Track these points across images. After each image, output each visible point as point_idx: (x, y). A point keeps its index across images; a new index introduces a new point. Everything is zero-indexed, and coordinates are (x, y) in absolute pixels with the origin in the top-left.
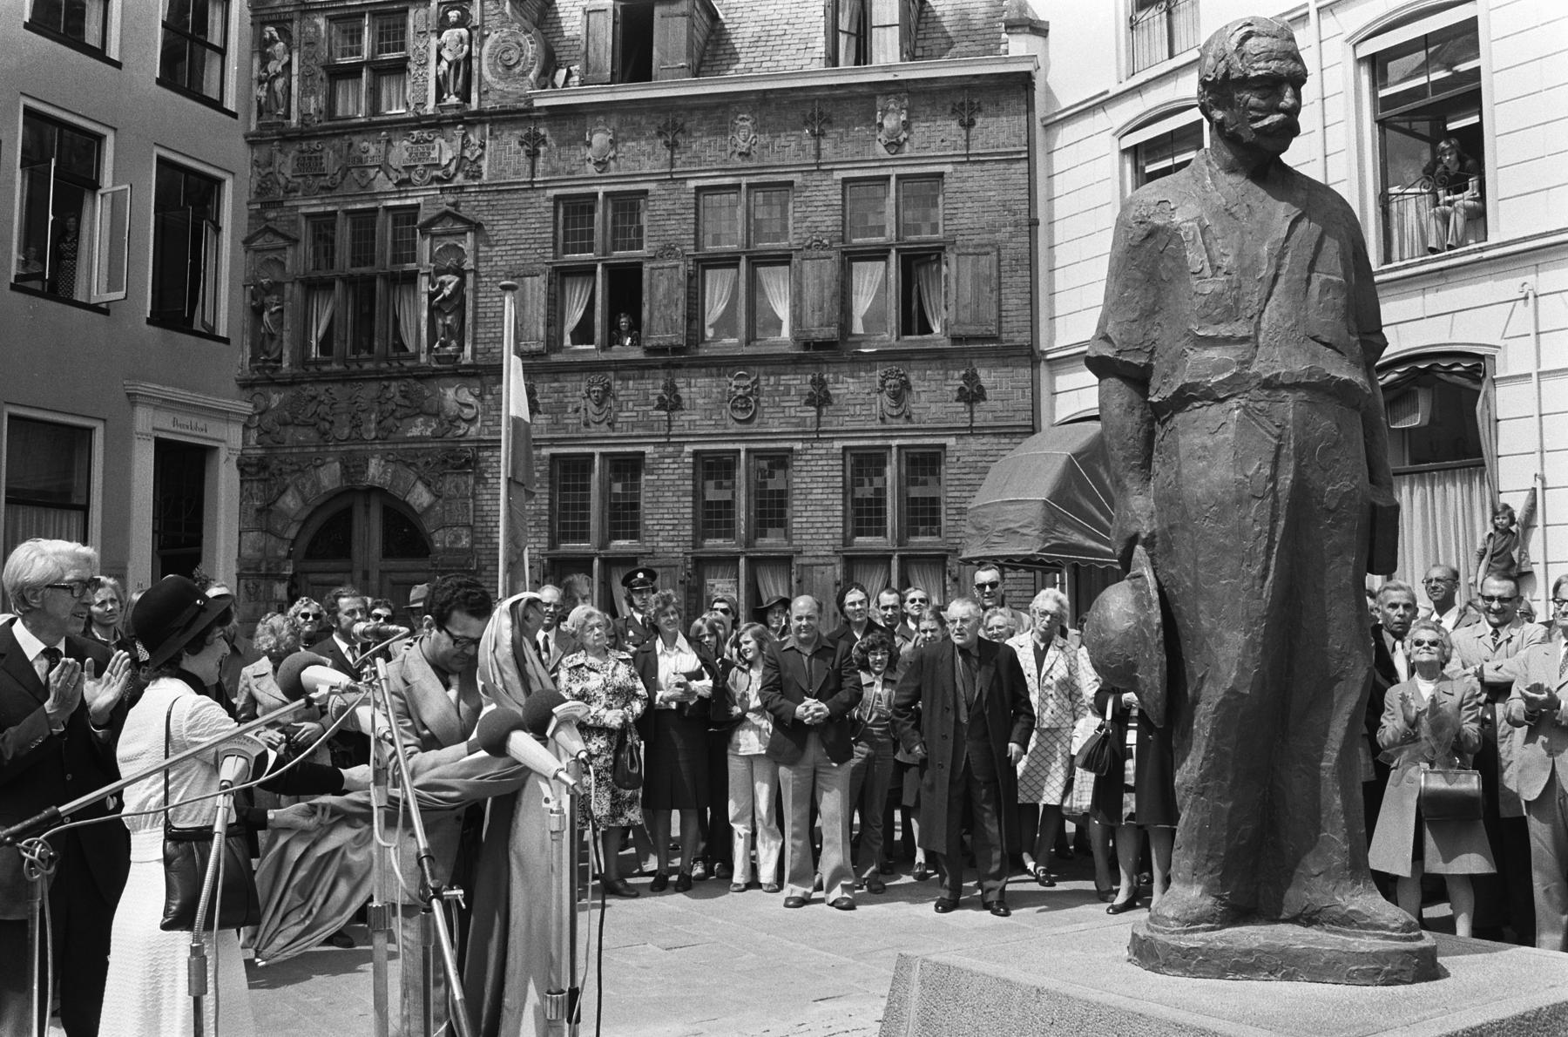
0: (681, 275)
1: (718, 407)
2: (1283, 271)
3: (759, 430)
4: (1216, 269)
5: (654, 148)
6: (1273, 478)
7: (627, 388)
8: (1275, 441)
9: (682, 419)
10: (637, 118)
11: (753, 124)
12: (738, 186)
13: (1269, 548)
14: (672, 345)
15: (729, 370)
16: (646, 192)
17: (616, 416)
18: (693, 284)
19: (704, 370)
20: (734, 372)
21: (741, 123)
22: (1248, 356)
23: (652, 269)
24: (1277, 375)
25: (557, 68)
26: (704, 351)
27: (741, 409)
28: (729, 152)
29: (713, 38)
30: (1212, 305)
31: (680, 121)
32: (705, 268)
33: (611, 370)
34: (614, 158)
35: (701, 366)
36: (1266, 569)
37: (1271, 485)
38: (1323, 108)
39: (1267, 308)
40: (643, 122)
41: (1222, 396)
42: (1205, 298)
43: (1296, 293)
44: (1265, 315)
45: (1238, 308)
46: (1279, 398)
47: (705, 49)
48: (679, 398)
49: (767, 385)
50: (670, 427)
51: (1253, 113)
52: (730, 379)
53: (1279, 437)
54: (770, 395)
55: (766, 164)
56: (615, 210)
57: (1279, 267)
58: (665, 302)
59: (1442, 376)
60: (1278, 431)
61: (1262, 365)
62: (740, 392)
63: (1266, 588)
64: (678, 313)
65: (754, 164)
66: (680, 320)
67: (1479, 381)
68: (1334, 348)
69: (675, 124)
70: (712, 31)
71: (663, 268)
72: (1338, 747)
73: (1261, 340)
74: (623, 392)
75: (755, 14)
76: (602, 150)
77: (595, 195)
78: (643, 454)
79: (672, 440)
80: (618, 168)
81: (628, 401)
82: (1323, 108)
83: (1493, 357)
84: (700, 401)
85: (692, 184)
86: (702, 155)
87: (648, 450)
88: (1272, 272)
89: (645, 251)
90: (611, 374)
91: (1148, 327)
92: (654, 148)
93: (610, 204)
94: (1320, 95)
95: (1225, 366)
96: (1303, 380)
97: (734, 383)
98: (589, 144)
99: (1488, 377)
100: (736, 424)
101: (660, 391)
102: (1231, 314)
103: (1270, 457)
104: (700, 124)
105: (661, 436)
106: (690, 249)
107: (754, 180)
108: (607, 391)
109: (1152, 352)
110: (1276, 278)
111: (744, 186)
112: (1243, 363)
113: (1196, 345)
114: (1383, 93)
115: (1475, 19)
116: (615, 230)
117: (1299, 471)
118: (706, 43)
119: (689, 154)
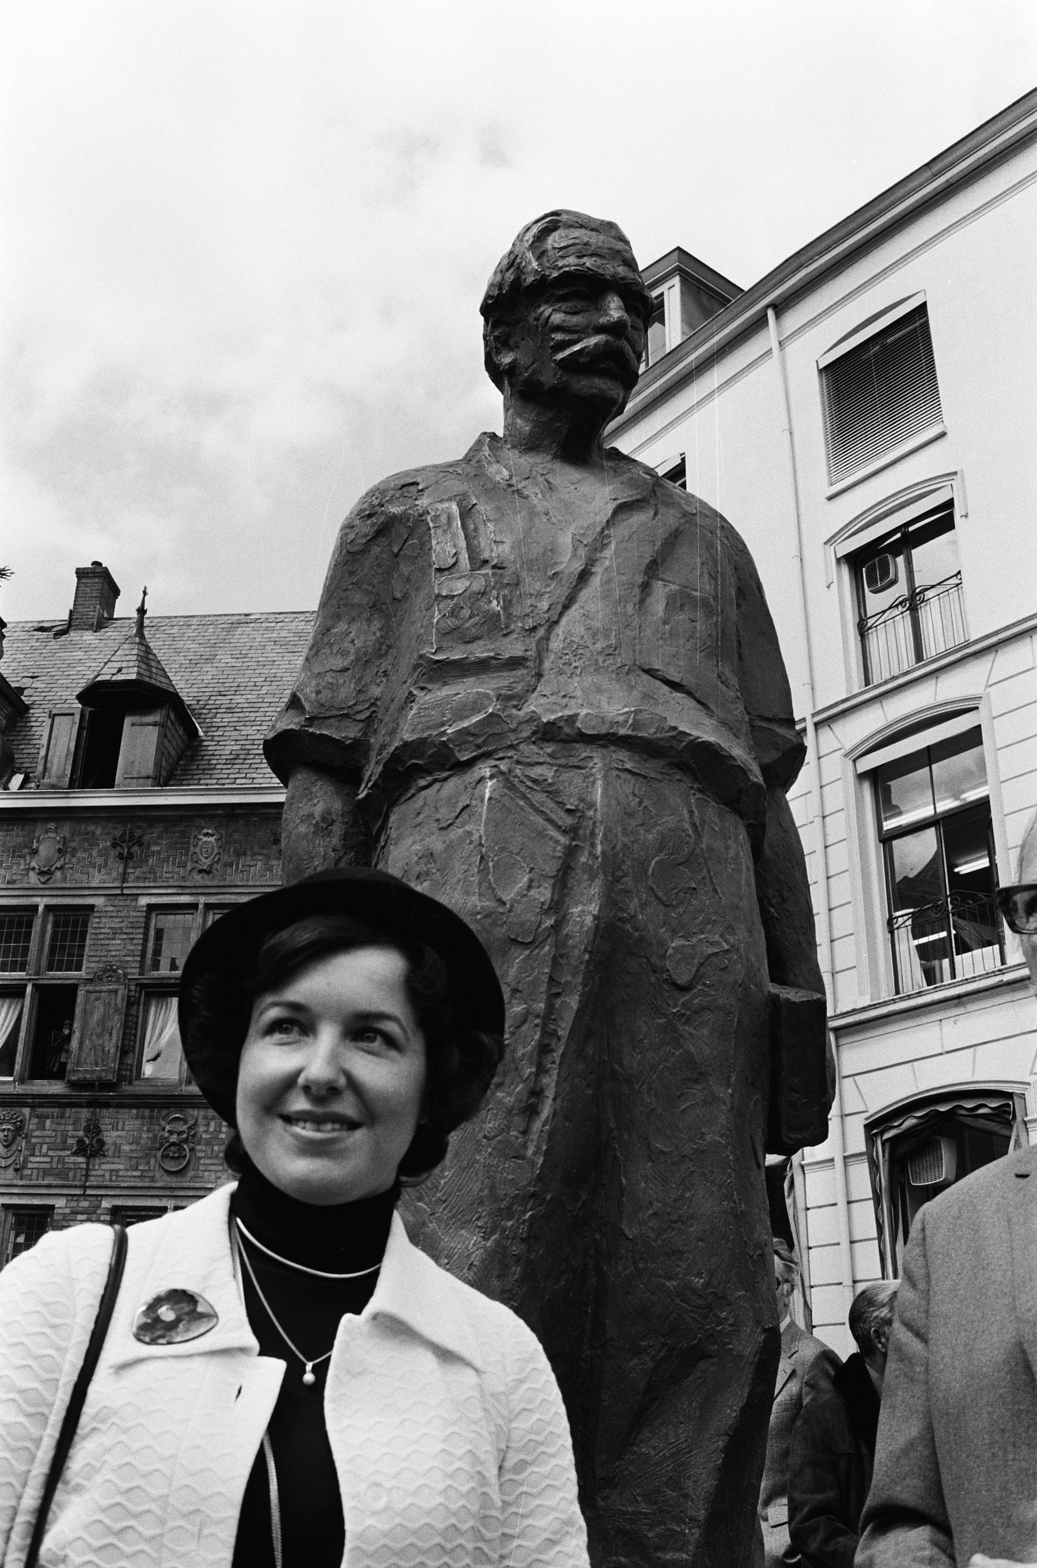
0: (119, 1000)
1: (147, 1155)
2: (598, 569)
3: (192, 1185)
4: (478, 562)
5: (106, 861)
6: (557, 907)
7: (44, 1129)
8: (563, 840)
9: (102, 1168)
10: (91, 828)
11: (217, 840)
12: (194, 906)
13: (544, 1049)
14: (100, 1079)
15: (164, 1112)
16: (91, 907)
17: (26, 1161)
18: (133, 1011)
19: (134, 1111)
20: (168, 1115)
21: (205, 839)
22: (519, 688)
23: (88, 992)
24: (572, 719)
25: (14, 773)
26: (138, 1088)
27: (173, 1158)
28: (189, 867)
29: (188, 753)
30: (466, 613)
31: (138, 833)
32: (149, 996)
33: (26, 1105)
34: (61, 868)
35: (131, 1107)
36: (536, 1093)
37: (549, 922)
38: (824, 827)
39: (564, 621)
40: (98, 832)
41: (464, 757)
42: (451, 603)
43: (622, 600)
44: (560, 630)
45: (509, 616)
46: (573, 761)
47: (177, 763)
48: (101, 1143)
49: (206, 1132)
50: (87, 1176)
51: (559, 337)
52: (163, 1123)
53: (572, 832)
54: (208, 1143)
55: (227, 883)
56: (56, 925)
57: (591, 562)
58: (99, 1030)
59: (968, 1121)
60: (569, 821)
61: (542, 701)
62: (174, 1138)
63: (534, 1136)
64: (112, 1044)
65: (215, 883)
66: (113, 1051)
67: (1009, 1125)
68: (689, 694)
69: (132, 836)
70: (188, 747)
71: (100, 992)
72: (702, 1514)
73: (547, 665)
74: (36, 1133)
75: (238, 733)
76: (48, 859)
77: (36, 907)
78: (52, 1207)
79: (89, 1192)
80: (65, 879)
81: (42, 1144)
82: (824, 827)
83: (1022, 1096)
84: (126, 1148)
85: (144, 901)
86: (158, 870)
87: (60, 1203)
88: (578, 566)
89: (83, 974)
90: (26, 1111)
91: (367, 679)
92: (106, 861)
93: (51, 918)
94: (819, 812)
95: (475, 707)
96: (622, 732)
97: (168, 1128)
98: (35, 852)
99: (1019, 1119)
100: (168, 1178)
101: (81, 1133)
102: (494, 626)
103: (551, 868)
104: (160, 837)
105: (76, 1187)
106: (134, 972)
107: (213, 900)
108: (19, 1129)
109: (369, 721)
110: (584, 576)
111: (201, 906)
112: (510, 698)
113: (431, 680)
114: (888, 825)
115: (978, 727)
116: (53, 948)
117: (611, 900)
118: (180, 758)
119: (144, 869)
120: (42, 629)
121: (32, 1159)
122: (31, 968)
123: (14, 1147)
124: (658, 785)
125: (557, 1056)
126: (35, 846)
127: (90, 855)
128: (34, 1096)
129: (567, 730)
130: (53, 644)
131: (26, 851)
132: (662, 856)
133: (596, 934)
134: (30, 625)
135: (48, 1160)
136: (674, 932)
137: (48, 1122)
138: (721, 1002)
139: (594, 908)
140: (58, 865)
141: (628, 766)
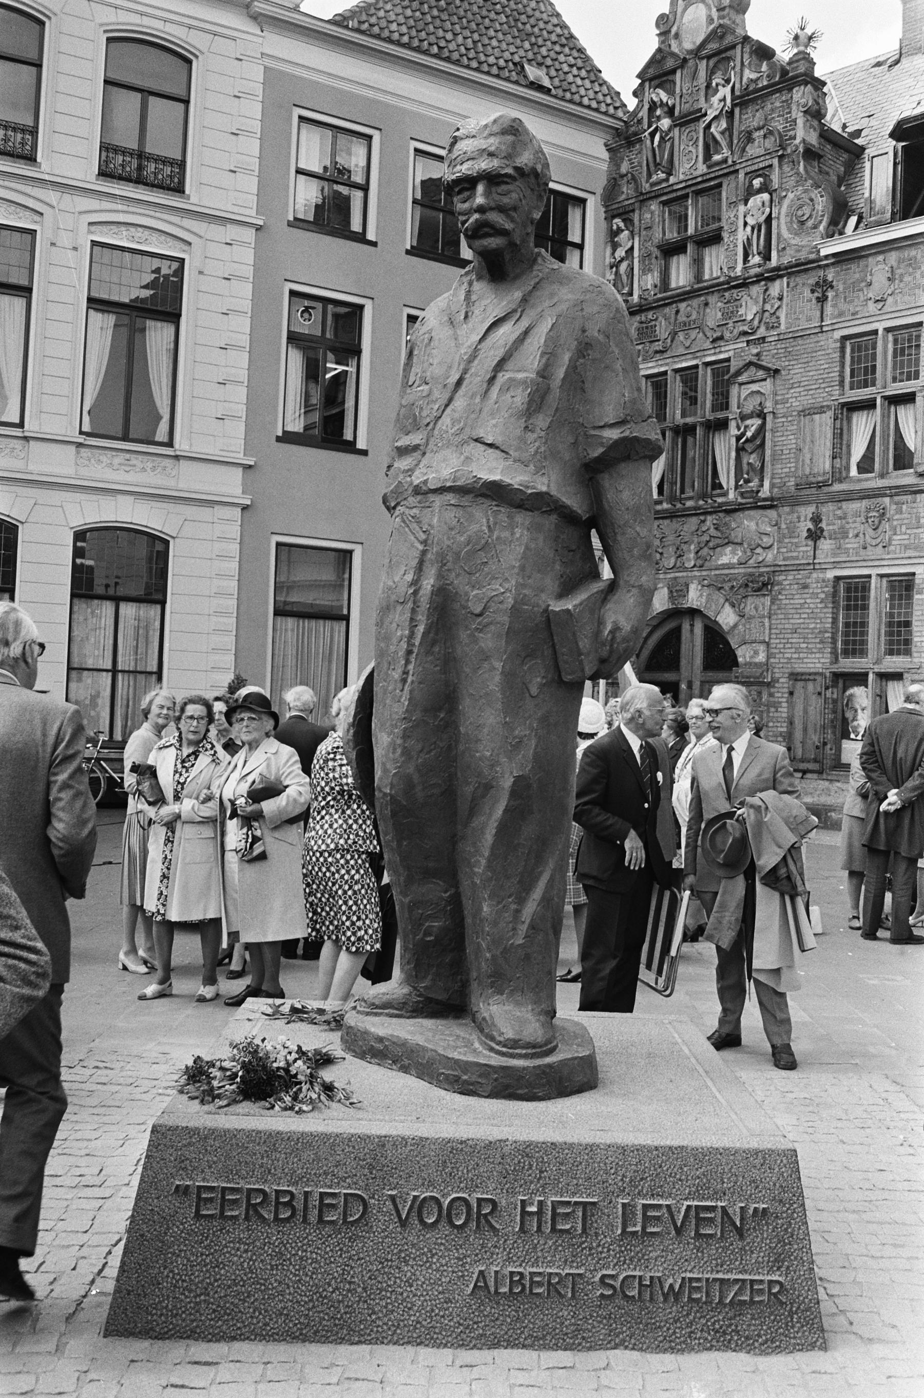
7: (901, 513)
8: (421, 547)
13: (409, 652)
17: (890, 539)
25: (848, 217)
33: (885, 495)
46: (427, 504)
53: (425, 542)
56: (896, 341)
60: (423, 537)
96: (448, 484)
117: (440, 576)
120: (879, 64)
121: (895, 537)
122: (879, 383)
123: (880, 529)
124: (469, 509)
126: (869, 278)
127: (915, 278)
128: (890, 488)
129: (424, 488)
130: (888, 76)
131: (863, 284)
135: (906, 537)
137: (904, 507)
138: (499, 619)
139: (432, 581)
140: (890, 292)
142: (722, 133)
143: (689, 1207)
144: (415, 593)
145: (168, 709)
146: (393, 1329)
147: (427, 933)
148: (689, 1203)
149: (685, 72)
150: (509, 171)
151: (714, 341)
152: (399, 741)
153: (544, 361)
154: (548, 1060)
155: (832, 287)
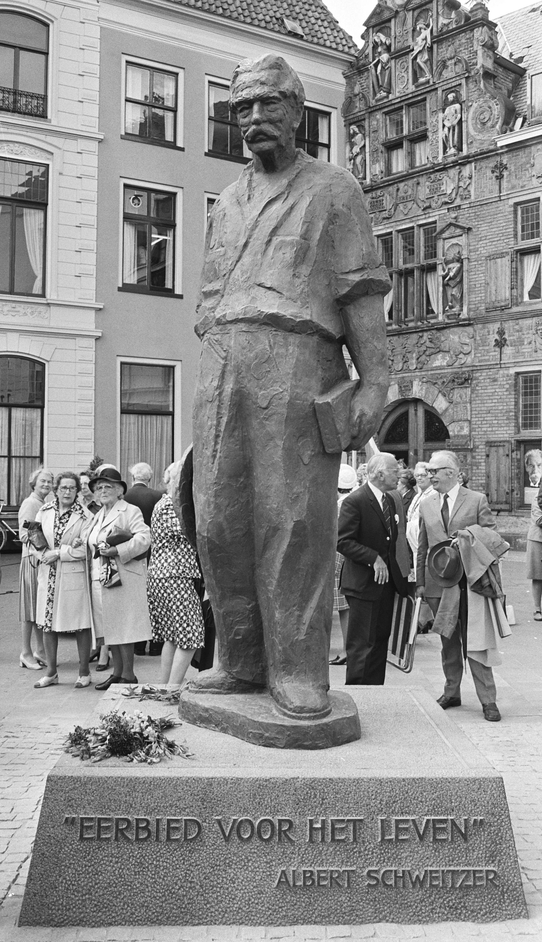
13: (217, 436)
25: (516, 118)
37: (217, 393)
46: (226, 331)
53: (225, 358)
96: (240, 317)
103: (219, 373)
120: (534, 10)
124: (256, 334)
125: (221, 438)
126: (532, 161)
129: (224, 320)
131: (528, 165)
132: (256, 361)
133: (232, 394)
134: (526, 10)
136: (261, 388)
141: (244, 329)
142: (425, 62)
143: (428, 821)
144: (220, 394)
145: (49, 482)
146: (222, 913)
147: (237, 634)
148: (428, 818)
149: (397, 20)
150: (276, 94)
151: (424, 209)
152: (212, 499)
153: (305, 227)
154: (325, 720)
155: (506, 168)
